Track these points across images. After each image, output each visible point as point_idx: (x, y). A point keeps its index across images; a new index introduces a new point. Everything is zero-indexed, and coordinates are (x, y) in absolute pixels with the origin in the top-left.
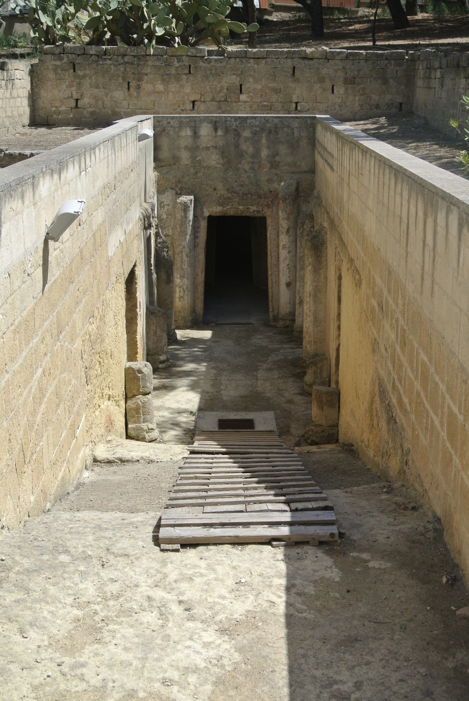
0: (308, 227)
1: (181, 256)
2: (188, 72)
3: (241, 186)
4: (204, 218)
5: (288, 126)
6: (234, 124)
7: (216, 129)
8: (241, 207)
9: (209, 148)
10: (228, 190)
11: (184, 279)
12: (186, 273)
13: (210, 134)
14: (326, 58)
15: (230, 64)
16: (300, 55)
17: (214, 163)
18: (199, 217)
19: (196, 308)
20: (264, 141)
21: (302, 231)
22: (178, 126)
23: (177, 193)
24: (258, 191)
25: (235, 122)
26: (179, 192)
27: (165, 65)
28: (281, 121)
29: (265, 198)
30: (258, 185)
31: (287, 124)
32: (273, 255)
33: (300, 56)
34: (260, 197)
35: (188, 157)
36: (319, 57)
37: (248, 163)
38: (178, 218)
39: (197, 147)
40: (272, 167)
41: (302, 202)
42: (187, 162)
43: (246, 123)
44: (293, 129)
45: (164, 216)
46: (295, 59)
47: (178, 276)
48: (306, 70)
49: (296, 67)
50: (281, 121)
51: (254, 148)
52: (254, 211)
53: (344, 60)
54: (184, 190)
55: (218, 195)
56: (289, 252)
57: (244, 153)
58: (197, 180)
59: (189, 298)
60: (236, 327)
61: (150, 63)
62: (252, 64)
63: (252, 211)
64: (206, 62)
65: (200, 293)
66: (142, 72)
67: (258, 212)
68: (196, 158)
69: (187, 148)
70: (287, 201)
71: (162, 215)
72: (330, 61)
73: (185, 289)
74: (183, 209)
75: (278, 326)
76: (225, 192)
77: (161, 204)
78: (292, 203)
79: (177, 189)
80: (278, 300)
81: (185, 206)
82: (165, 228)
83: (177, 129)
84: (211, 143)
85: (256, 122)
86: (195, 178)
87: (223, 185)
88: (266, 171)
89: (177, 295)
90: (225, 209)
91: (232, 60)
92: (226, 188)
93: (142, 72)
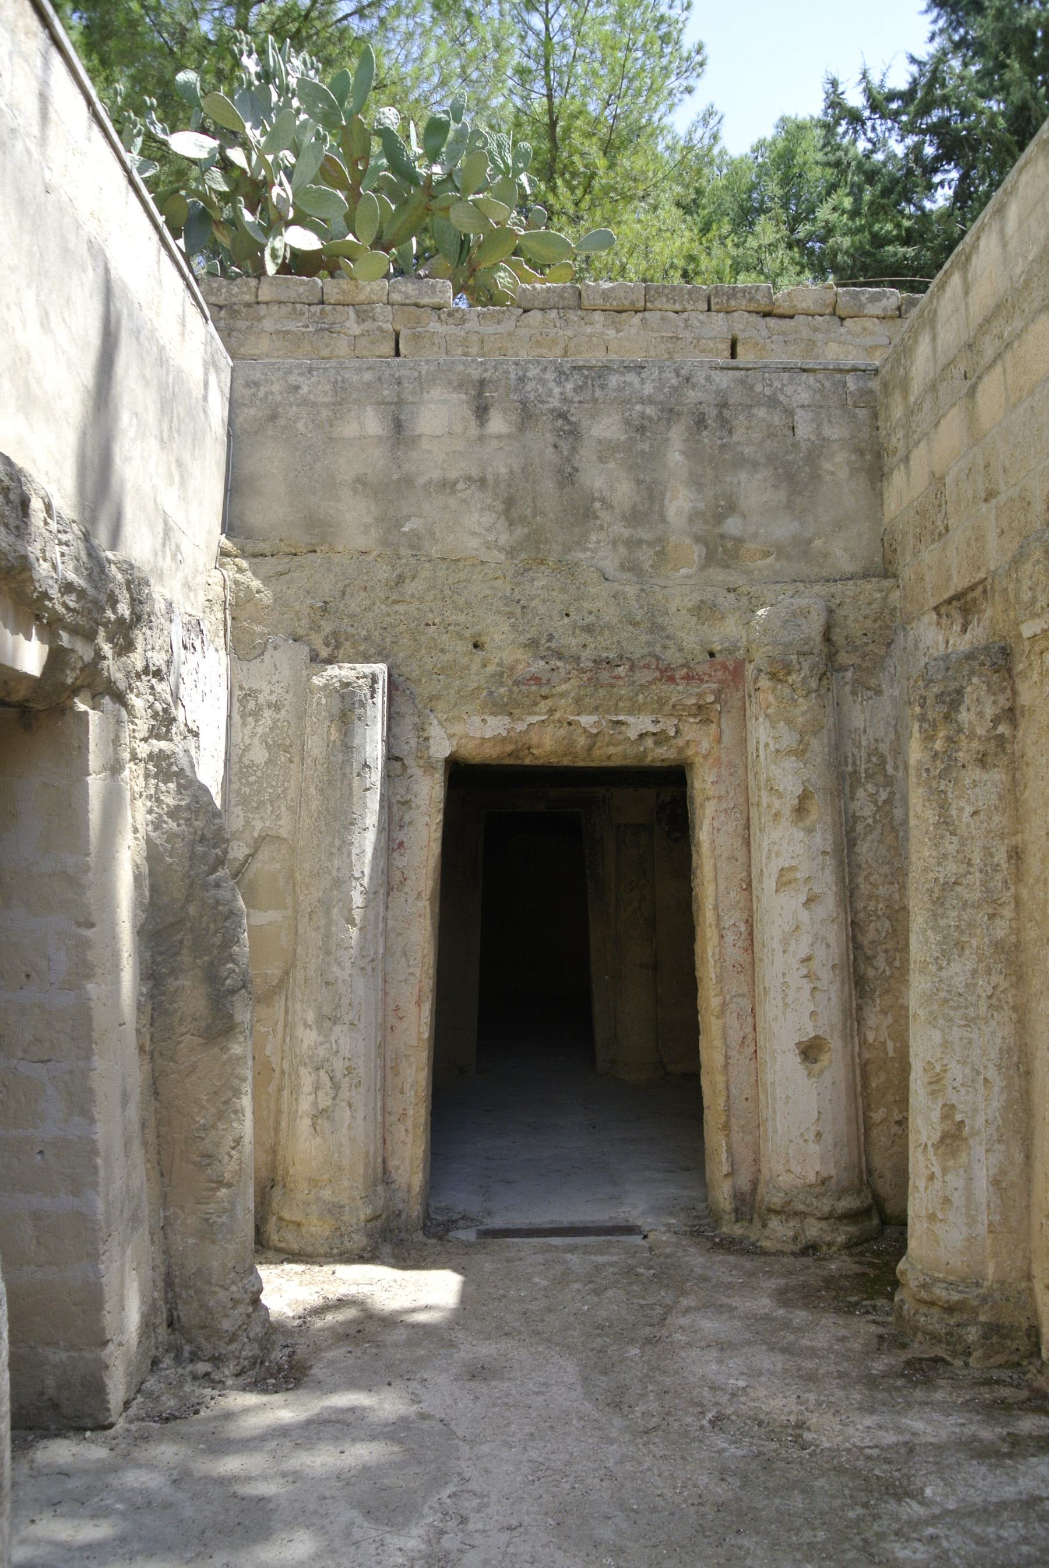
0: (981, 714)
1: (323, 922)
2: (393, 353)
3: (589, 629)
4: (429, 767)
5: (772, 402)
6: (557, 390)
7: (482, 412)
8: (587, 720)
9: (455, 483)
10: (533, 644)
11: (338, 1029)
12: (345, 1001)
13: (458, 429)
14: (834, 314)
15: (528, 326)
16: (750, 300)
17: (473, 543)
18: (409, 761)
19: (393, 1163)
20: (675, 456)
21: (950, 739)
22: (328, 399)
23: (314, 658)
24: (658, 649)
25: (559, 383)
26: (324, 653)
27: (317, 331)
28: (742, 382)
29: (688, 678)
30: (656, 628)
31: (768, 391)
32: (727, 923)
33: (752, 307)
34: (667, 675)
35: (369, 519)
36: (813, 308)
37: (614, 543)
38: (316, 751)
39: (407, 481)
40: (710, 560)
41: (848, 688)
42: (361, 542)
43: (602, 387)
44: (790, 413)
45: (259, 755)
46: (735, 314)
47: (311, 1016)
48: (774, 346)
49: (741, 336)
50: (742, 382)
51: (639, 482)
52: (642, 736)
53: (892, 318)
54: (347, 644)
55: (491, 669)
56: (809, 902)
57: (597, 505)
58: (400, 608)
59: (360, 1115)
60: (573, 1249)
61: (268, 325)
62: (598, 327)
63: (633, 735)
64: (451, 320)
65: (410, 1094)
66: (242, 351)
67: (660, 738)
68: (399, 524)
69: (365, 484)
70: (793, 678)
71: (247, 748)
72: (848, 322)
73: (338, 1074)
74: (336, 710)
75: (766, 1244)
76: (520, 654)
77: (243, 700)
78: (814, 684)
79: (318, 641)
80: (756, 1125)
81: (343, 697)
82: (261, 804)
83: (325, 413)
84: (463, 465)
85: (643, 382)
86: (395, 602)
87: (513, 626)
88: (688, 577)
89: (305, 1104)
90: (521, 727)
91: (536, 315)
92: (523, 639)
93: (242, 351)
